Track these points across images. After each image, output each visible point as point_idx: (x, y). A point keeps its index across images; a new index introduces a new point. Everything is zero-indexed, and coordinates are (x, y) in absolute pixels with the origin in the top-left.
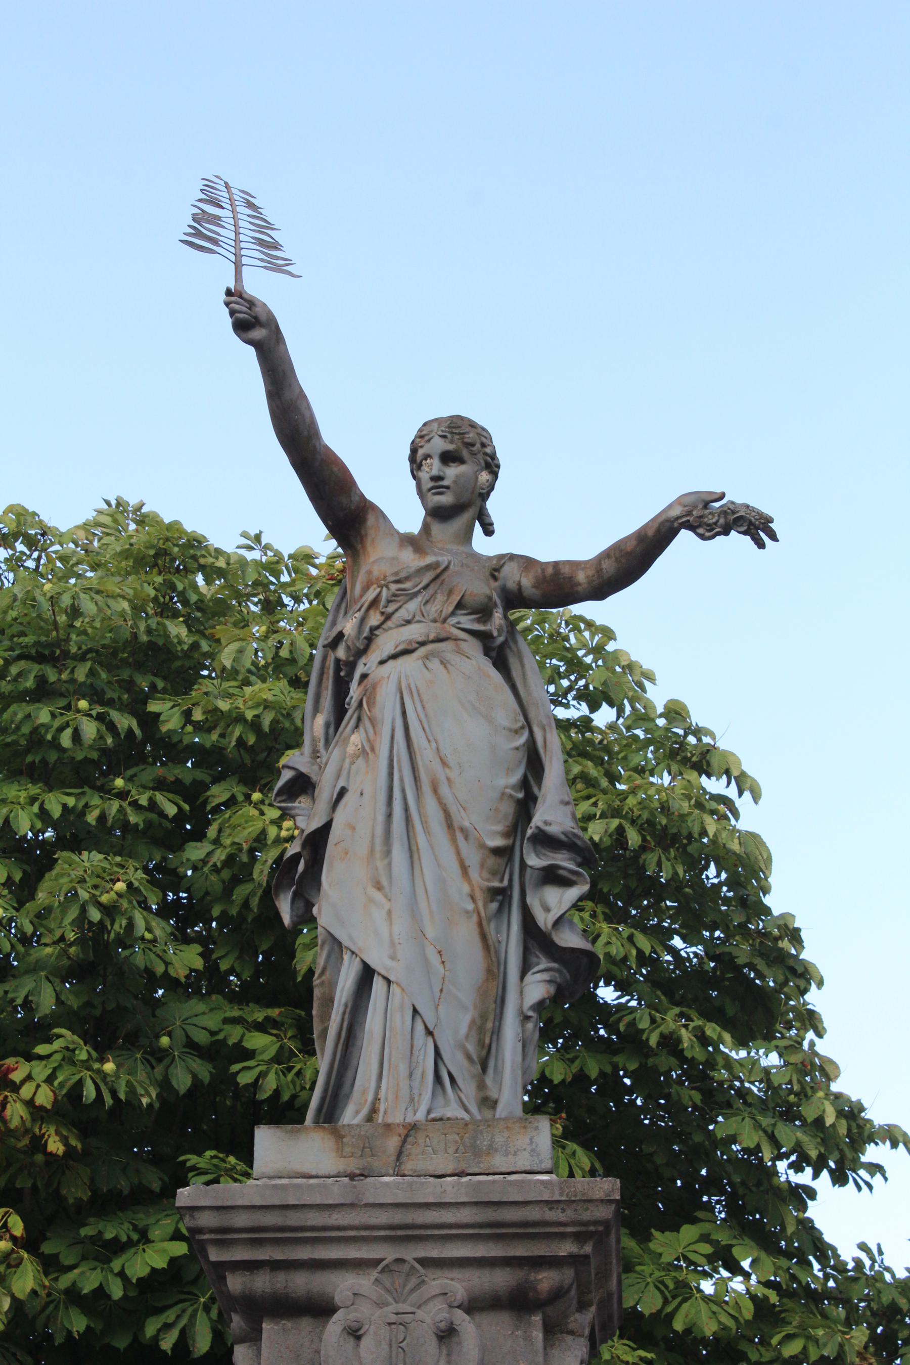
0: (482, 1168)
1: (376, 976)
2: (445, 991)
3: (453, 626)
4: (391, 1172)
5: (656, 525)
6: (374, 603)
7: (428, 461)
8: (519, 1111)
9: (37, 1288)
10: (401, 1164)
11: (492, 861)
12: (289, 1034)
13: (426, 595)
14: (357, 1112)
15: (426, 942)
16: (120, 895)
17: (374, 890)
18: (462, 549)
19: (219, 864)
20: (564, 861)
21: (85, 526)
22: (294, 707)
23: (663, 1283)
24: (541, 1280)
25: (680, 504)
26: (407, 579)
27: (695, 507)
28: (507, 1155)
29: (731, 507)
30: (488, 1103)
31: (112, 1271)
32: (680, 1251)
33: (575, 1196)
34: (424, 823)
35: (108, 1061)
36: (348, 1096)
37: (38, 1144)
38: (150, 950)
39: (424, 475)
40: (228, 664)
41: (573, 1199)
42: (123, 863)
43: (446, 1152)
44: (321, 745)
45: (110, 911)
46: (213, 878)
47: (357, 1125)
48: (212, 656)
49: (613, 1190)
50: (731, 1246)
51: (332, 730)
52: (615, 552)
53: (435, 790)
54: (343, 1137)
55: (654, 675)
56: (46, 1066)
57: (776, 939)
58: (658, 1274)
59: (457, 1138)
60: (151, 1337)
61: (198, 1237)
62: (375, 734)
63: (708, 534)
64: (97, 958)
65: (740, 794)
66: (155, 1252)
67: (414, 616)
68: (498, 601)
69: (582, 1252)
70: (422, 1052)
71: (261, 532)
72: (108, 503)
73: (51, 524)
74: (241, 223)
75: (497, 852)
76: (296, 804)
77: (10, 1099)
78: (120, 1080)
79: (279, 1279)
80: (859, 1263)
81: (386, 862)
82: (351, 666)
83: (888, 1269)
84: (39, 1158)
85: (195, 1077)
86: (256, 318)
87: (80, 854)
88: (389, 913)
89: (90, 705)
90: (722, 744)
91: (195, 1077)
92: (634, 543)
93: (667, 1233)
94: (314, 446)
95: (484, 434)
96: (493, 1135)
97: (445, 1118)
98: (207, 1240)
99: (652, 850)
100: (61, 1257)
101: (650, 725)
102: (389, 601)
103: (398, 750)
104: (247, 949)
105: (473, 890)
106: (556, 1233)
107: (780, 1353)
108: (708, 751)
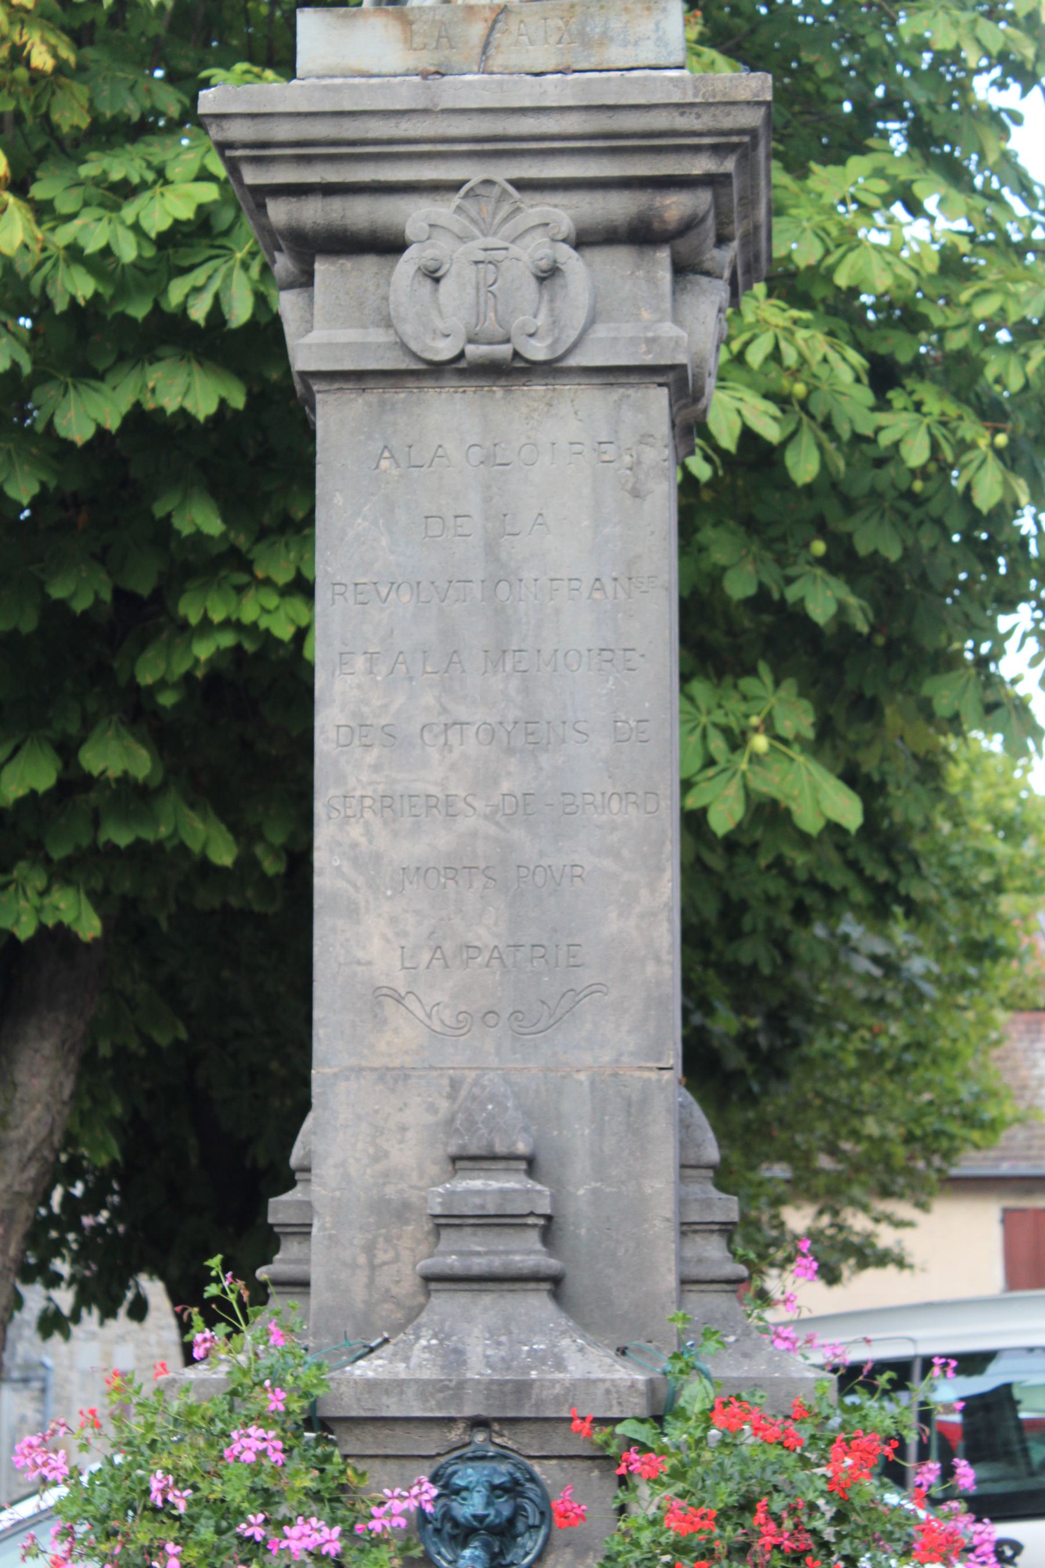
4: (475, 68)
10: (487, 58)
24: (669, 206)
28: (625, 46)
31: (123, 222)
33: (714, 97)
41: (711, 100)
43: (546, 42)
47: (430, 8)
49: (763, 89)
50: (912, 182)
54: (411, 23)
58: (818, 218)
59: (561, 23)
60: (178, 306)
69: (722, 170)
79: (334, 207)
84: (21, 73)
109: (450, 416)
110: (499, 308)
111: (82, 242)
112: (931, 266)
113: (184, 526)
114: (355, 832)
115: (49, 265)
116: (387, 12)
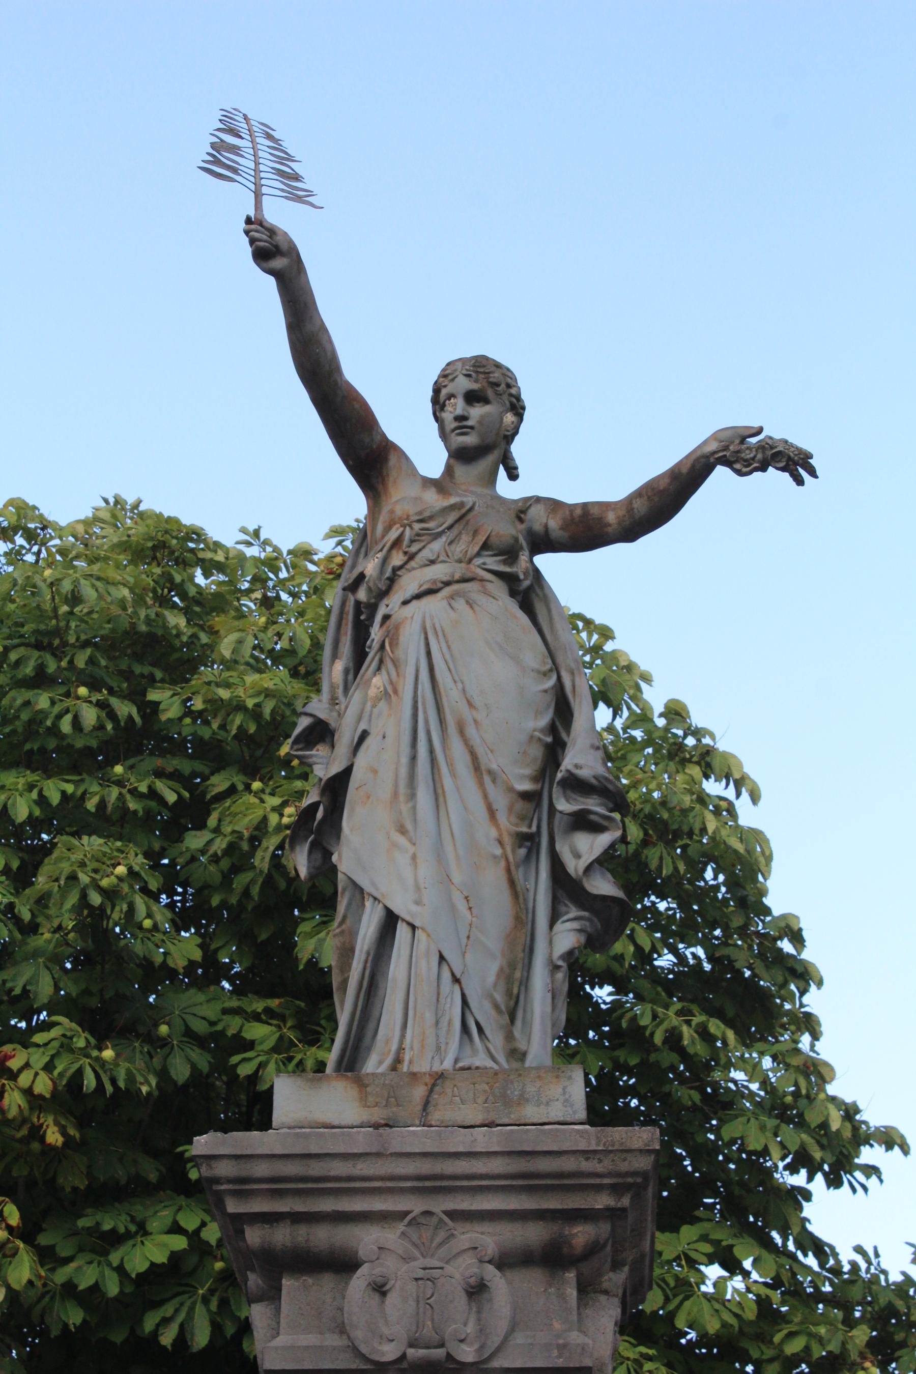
0: (513, 1118)
1: (400, 923)
2: (471, 939)
3: (479, 566)
4: (417, 1122)
5: (690, 462)
6: (397, 543)
7: (452, 401)
8: (548, 1061)
9: (34, 1279)
10: (427, 1114)
11: (520, 805)
12: (289, 1024)
13: (451, 535)
14: (380, 1063)
15: (452, 886)
16: (120, 879)
17: (398, 834)
18: (486, 491)
19: (219, 853)
20: (595, 805)
21: (87, 523)
22: (294, 696)
23: (664, 1280)
24: (576, 1234)
25: (716, 439)
26: (431, 518)
27: (732, 442)
28: (538, 1106)
29: (770, 442)
30: (517, 1055)
31: (109, 1264)
32: (680, 1249)
33: (613, 1146)
34: (451, 765)
35: (107, 1048)
36: (369, 1049)
37: (37, 1133)
38: (149, 939)
39: (448, 416)
40: (227, 654)
41: (610, 1148)
42: (123, 848)
44: (340, 691)
45: (110, 895)
46: (211, 868)
48: (211, 647)
49: (652, 1138)
51: (351, 677)
52: (648, 490)
53: (461, 731)
54: (367, 1086)
55: (651, 676)
56: (44, 1053)
57: (775, 939)
59: (487, 1088)
60: (150, 1333)
61: (215, 1187)
62: (398, 675)
63: (744, 470)
64: (97, 945)
65: (738, 795)
66: (155, 1245)
67: (438, 556)
68: (524, 544)
69: (619, 1205)
70: (449, 1000)
71: (260, 527)
72: (106, 501)
73: (51, 518)
74: (261, 154)
75: (526, 796)
76: (314, 752)
77: (7, 1087)
78: (119, 1069)
79: (301, 1232)
80: (854, 1266)
81: (410, 805)
82: (373, 608)
83: (884, 1272)
84: (36, 1146)
85: (194, 1067)
86: (277, 247)
87: (80, 838)
88: (414, 857)
89: (90, 692)
90: (722, 746)
91: (194, 1067)
92: (667, 481)
93: (667, 1234)
94: (336, 383)
95: (510, 374)
96: (524, 1085)
97: (473, 1067)
98: (224, 1190)
99: (655, 845)
100: (58, 1249)
101: (649, 726)
102: (412, 541)
103: (423, 690)
104: (245, 938)
105: (501, 835)
106: (593, 1185)
107: (782, 1351)
108: (708, 752)
110: (435, 1317)
111: (76, 1281)
112: (751, 1313)
115: (47, 1299)
116: (347, 1077)
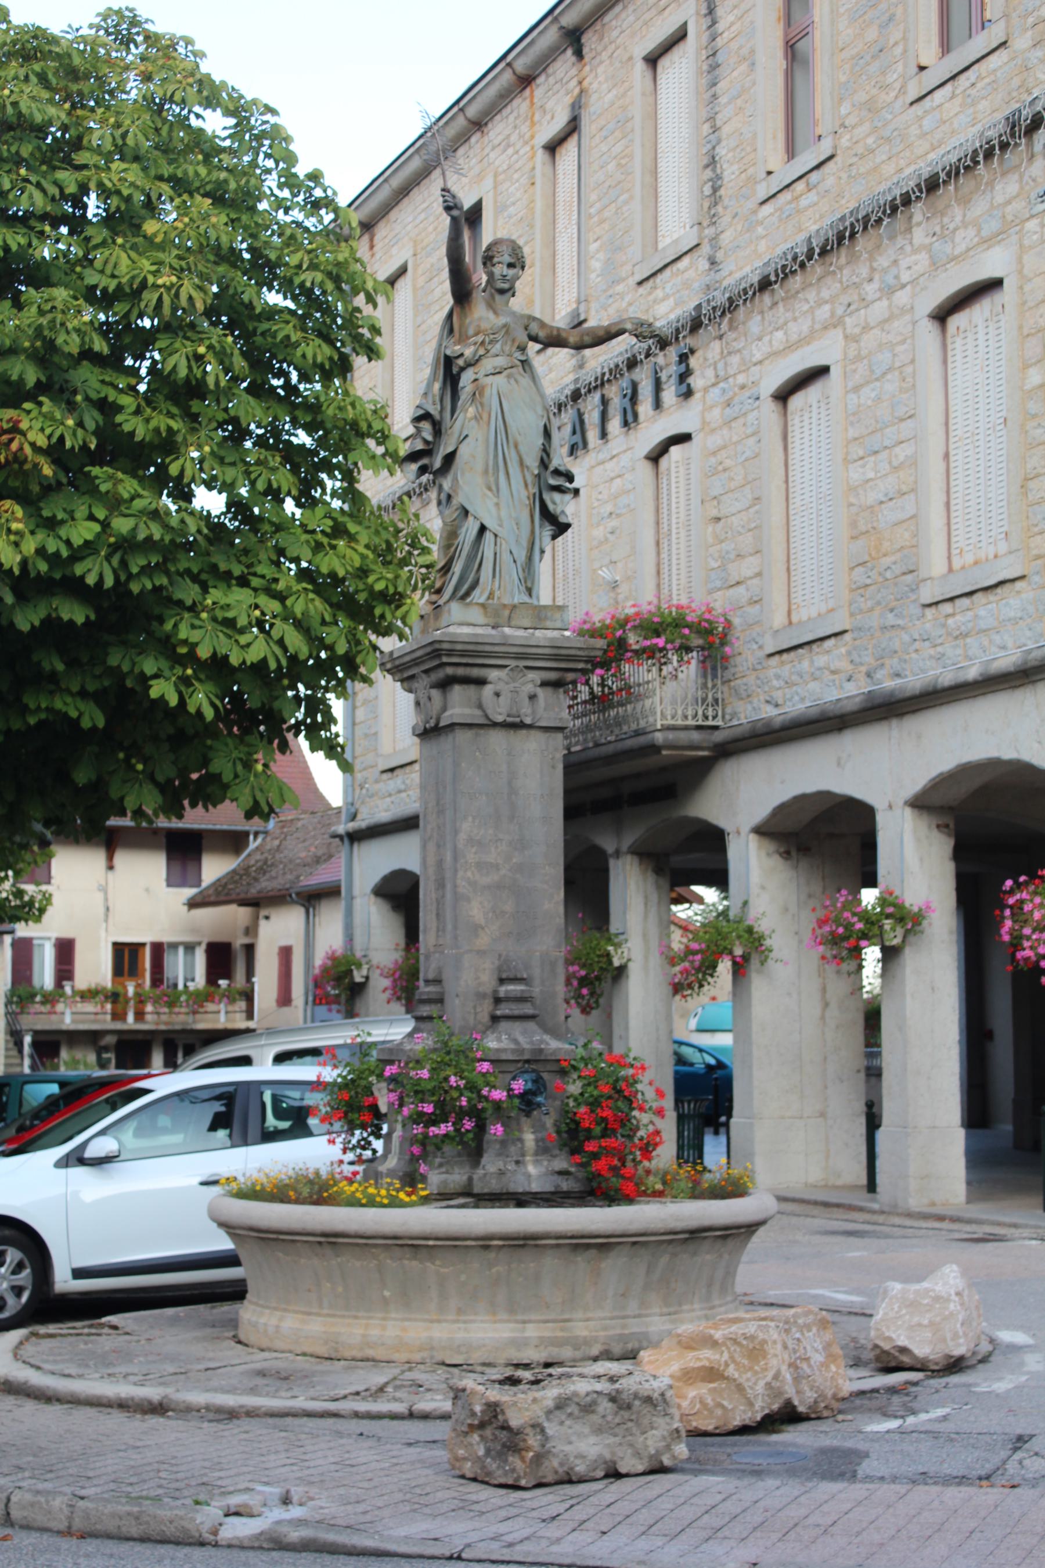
14: (481, 593)
109: (497, 739)
113: (46, 666)
114: (469, 874)
